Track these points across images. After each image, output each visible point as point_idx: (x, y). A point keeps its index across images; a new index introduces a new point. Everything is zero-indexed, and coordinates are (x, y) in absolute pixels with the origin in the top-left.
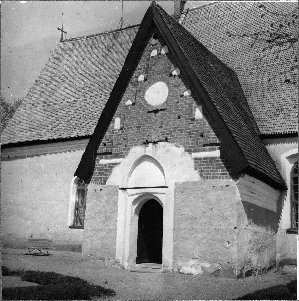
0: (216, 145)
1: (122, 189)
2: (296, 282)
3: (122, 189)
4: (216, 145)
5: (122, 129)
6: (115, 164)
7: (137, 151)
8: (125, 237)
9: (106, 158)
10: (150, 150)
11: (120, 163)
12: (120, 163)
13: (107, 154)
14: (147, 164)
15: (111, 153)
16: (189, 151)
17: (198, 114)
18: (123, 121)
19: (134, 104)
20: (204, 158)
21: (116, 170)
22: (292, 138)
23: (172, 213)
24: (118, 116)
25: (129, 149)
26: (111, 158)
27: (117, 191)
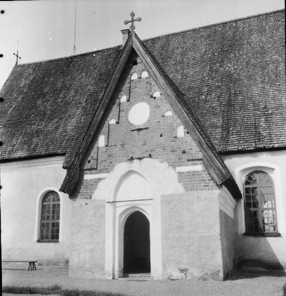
0: (201, 160)
6: (100, 179)
9: (91, 174)
11: (105, 178)
12: (105, 178)
16: (173, 165)
21: (101, 185)
22: (276, 155)
25: (114, 166)
26: (96, 173)
27: (103, 206)
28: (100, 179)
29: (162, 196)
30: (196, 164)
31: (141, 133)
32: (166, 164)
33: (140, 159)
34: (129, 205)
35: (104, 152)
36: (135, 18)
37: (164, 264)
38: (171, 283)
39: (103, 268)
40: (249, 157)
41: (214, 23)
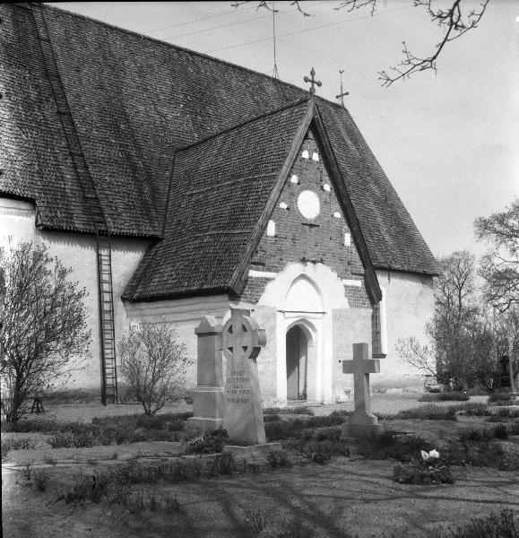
0: (361, 275)
1: (281, 311)
2: (288, 376)
3: (281, 311)
4: (361, 275)
5: (299, 184)
6: (268, 280)
7: (294, 269)
8: (464, 486)
9: (257, 270)
10: (309, 269)
11: (273, 279)
12: (273, 279)
13: (260, 265)
14: (303, 282)
15: (263, 264)
16: (342, 277)
17: (348, 239)
18: (277, 226)
19: (288, 209)
20: (352, 287)
21: (269, 287)
22: (402, 279)
23: (278, 354)
24: (283, 201)
25: (285, 265)
26: (263, 270)
27: (275, 314)
28: (268, 280)
29: (333, 310)
30: (356, 279)
31: (313, 230)
32: (335, 274)
33: (314, 262)
34: (298, 317)
35: (273, 243)
36: (310, 78)
37: (333, 387)
38: (338, 405)
39: (274, 395)
40: (78, 246)
41: (193, 49)
